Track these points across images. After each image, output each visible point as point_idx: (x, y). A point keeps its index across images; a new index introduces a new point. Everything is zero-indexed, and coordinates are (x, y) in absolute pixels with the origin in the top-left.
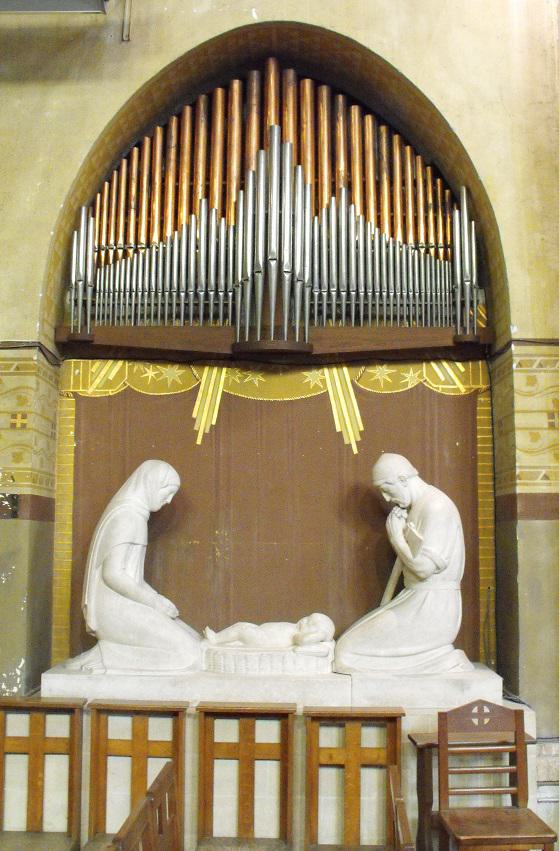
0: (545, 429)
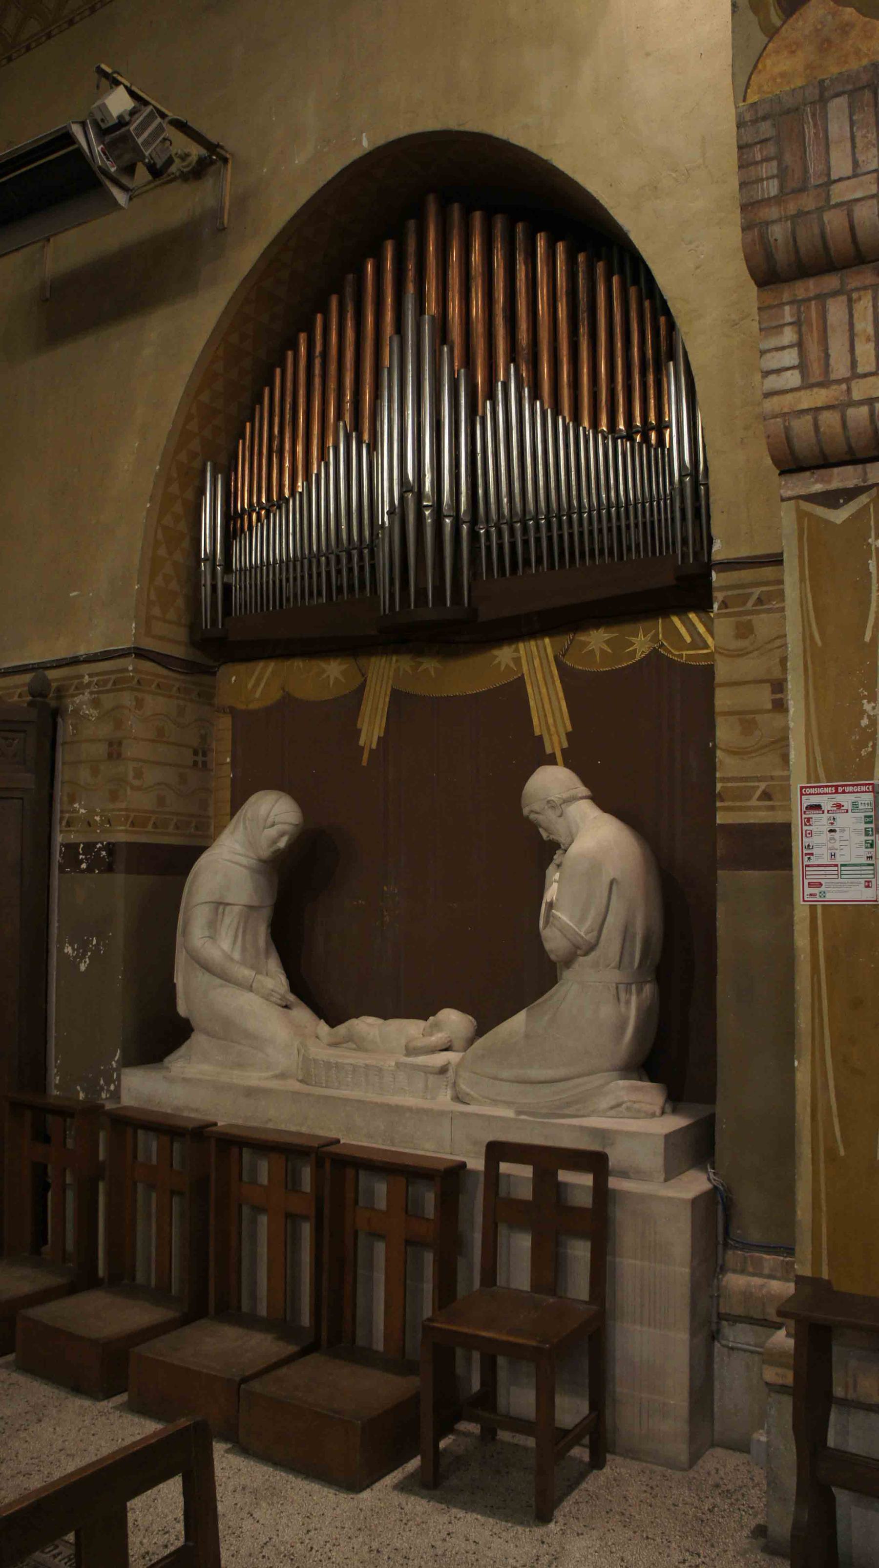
0: (769, 711)
